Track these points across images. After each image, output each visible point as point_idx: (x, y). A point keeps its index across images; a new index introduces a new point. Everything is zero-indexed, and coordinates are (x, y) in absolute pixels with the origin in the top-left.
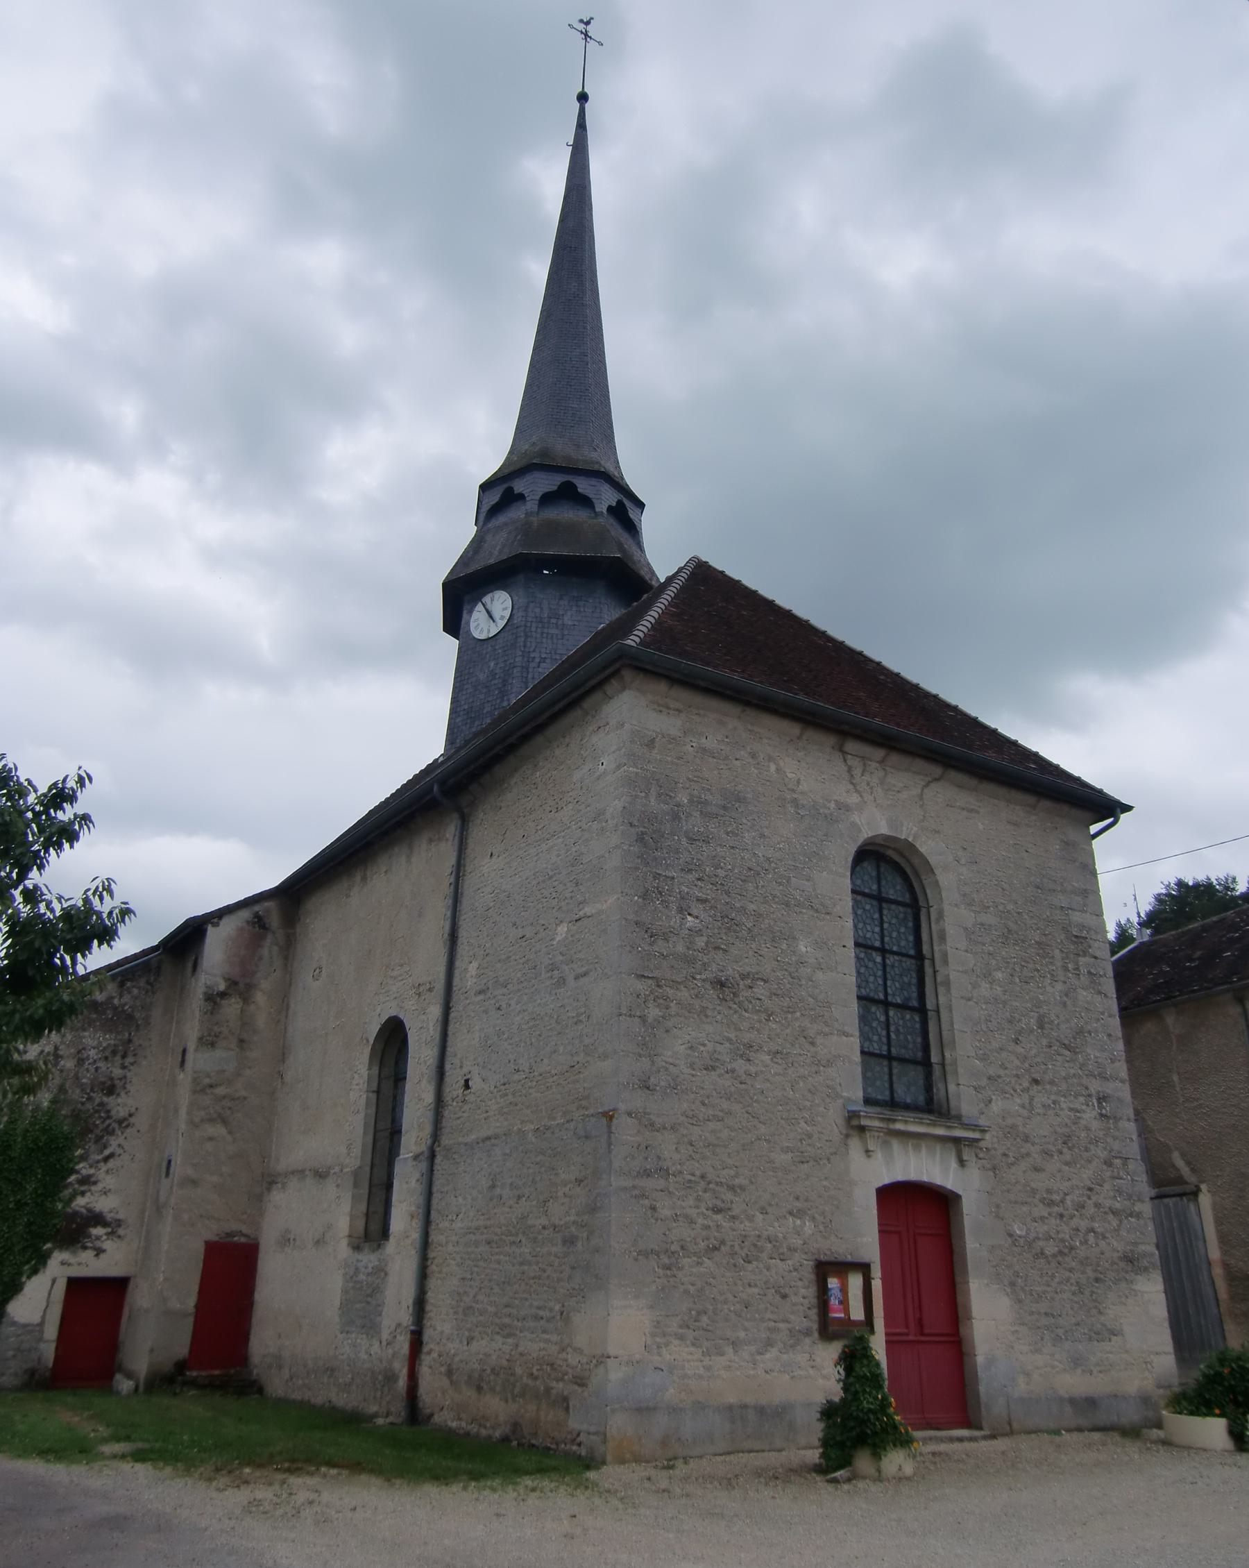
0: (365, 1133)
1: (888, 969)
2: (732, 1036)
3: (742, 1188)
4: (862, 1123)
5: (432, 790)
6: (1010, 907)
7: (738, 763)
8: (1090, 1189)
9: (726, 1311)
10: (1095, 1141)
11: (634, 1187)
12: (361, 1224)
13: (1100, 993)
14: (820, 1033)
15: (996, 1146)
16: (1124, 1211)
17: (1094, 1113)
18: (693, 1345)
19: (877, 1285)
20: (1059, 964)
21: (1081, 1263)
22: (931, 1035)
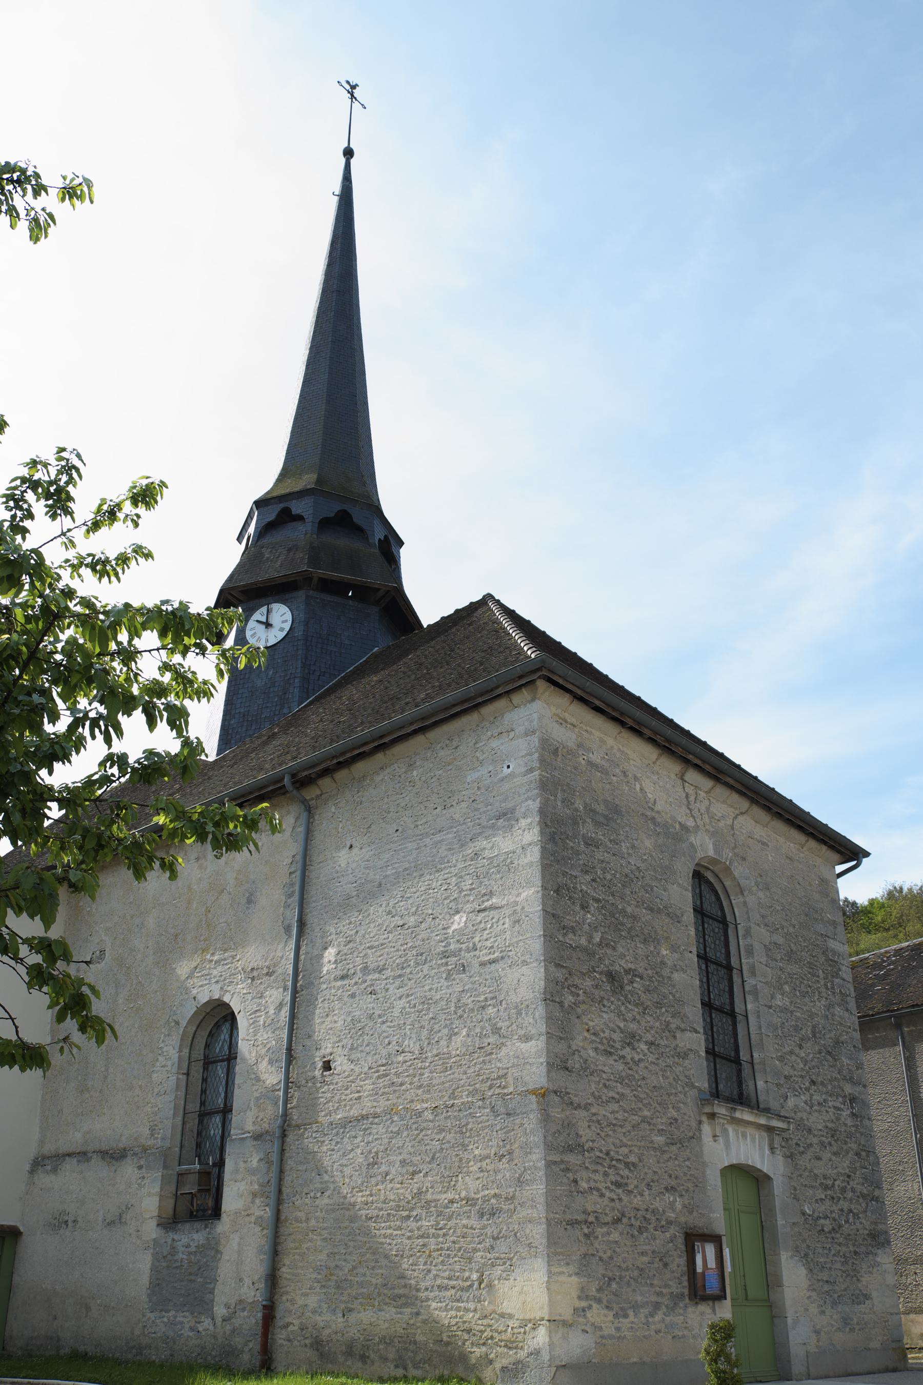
0: (175, 1115)
1: (710, 975)
2: (622, 1025)
3: (634, 1165)
4: (715, 1111)
5: (282, 779)
6: (791, 930)
7: (614, 778)
8: (849, 1176)
9: (628, 1277)
10: (850, 1135)
11: (562, 1162)
12: (170, 1204)
13: (847, 1010)
14: (678, 1028)
15: (792, 1136)
16: (869, 1195)
17: (848, 1112)
18: (607, 1307)
19: (727, 1252)
20: (822, 983)
21: (846, 1238)
22: (740, 1037)
